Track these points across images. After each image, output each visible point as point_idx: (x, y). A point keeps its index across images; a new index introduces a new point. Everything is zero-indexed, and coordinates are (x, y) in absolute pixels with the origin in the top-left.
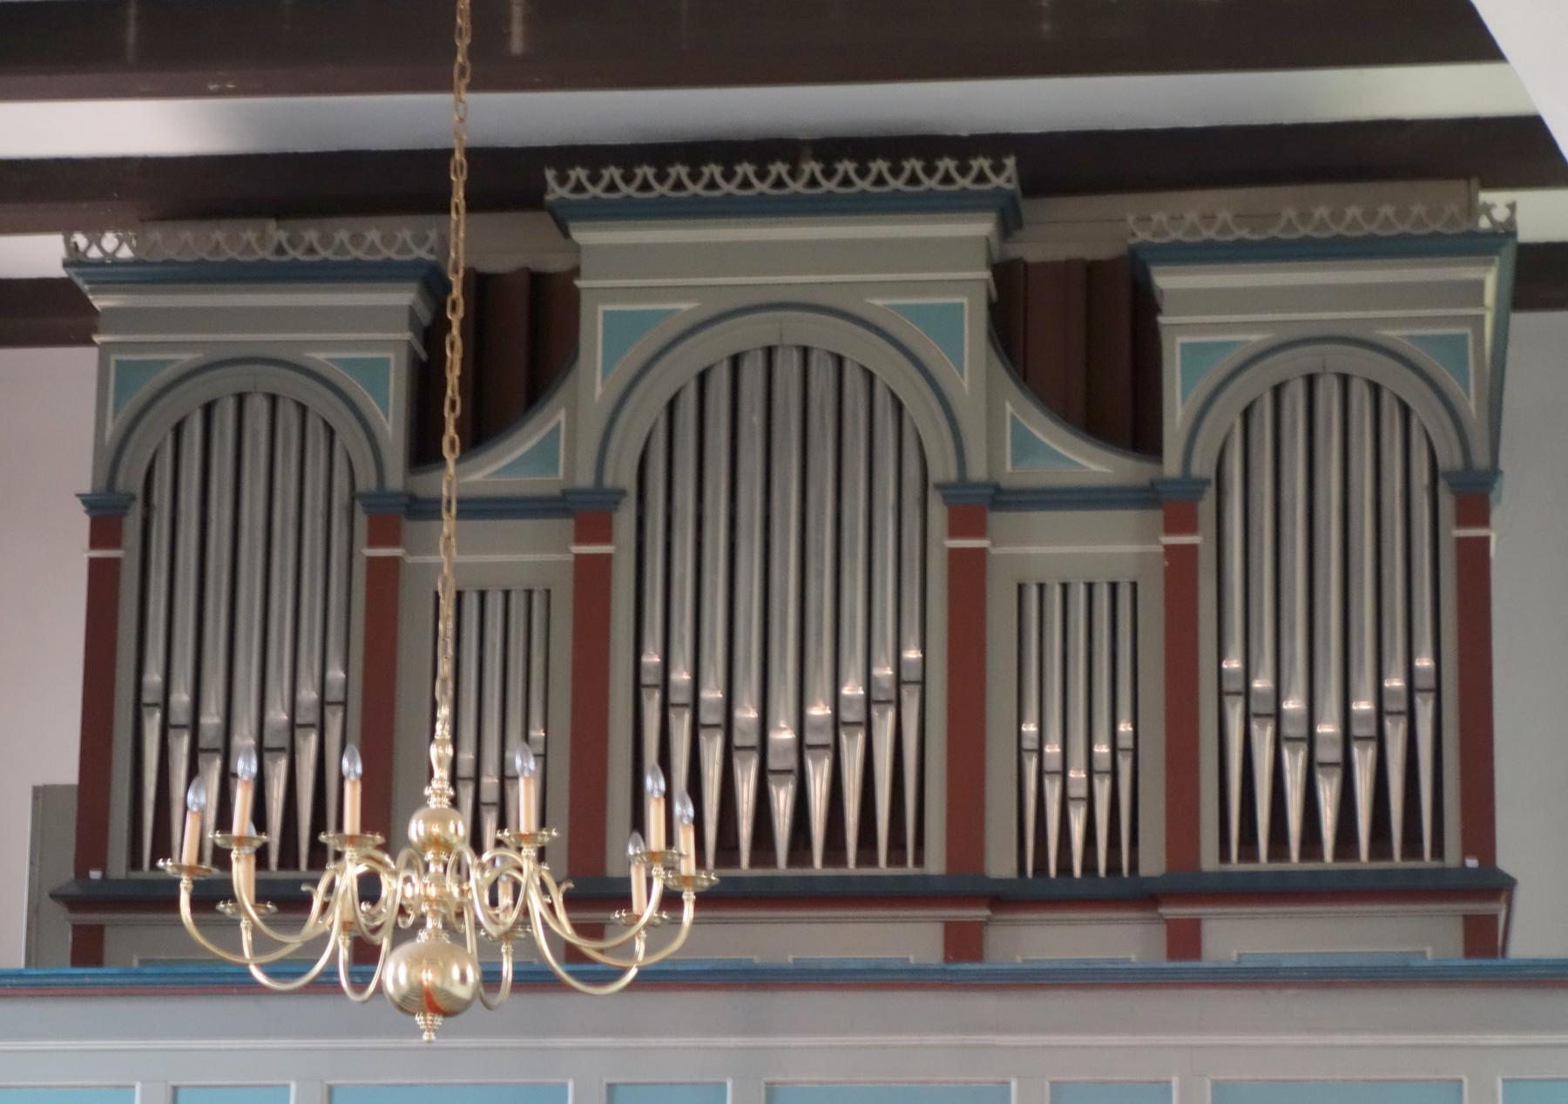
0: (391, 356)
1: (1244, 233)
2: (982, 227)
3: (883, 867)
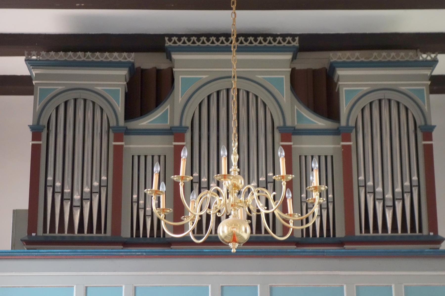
0: (424, 88)
1: (363, 59)
2: (288, 57)
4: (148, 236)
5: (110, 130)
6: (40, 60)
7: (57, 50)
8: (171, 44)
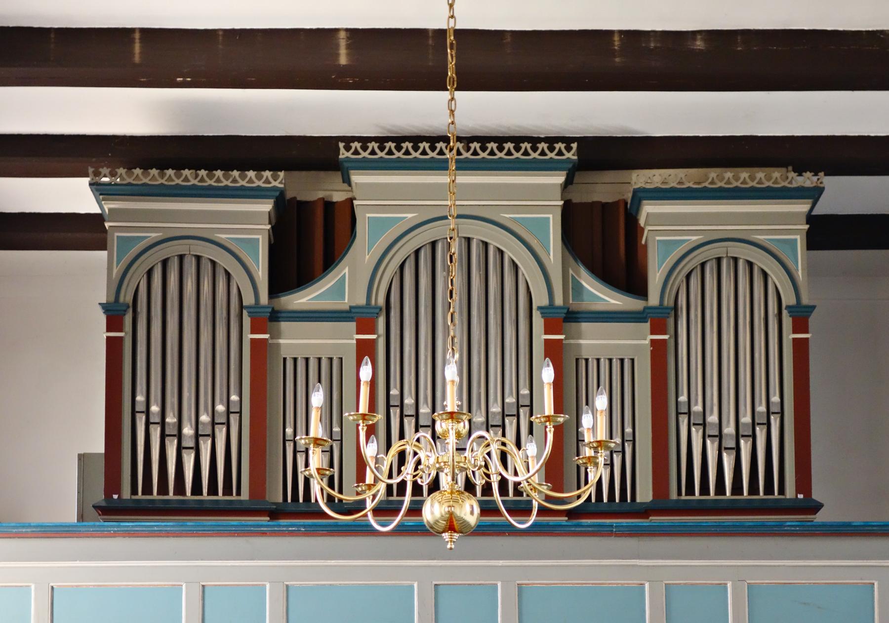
0: (798, 237)
3: (140, 495)
4: (301, 500)
5: (245, 312)
6: (116, 184)
7: (146, 166)
8: (349, 154)
